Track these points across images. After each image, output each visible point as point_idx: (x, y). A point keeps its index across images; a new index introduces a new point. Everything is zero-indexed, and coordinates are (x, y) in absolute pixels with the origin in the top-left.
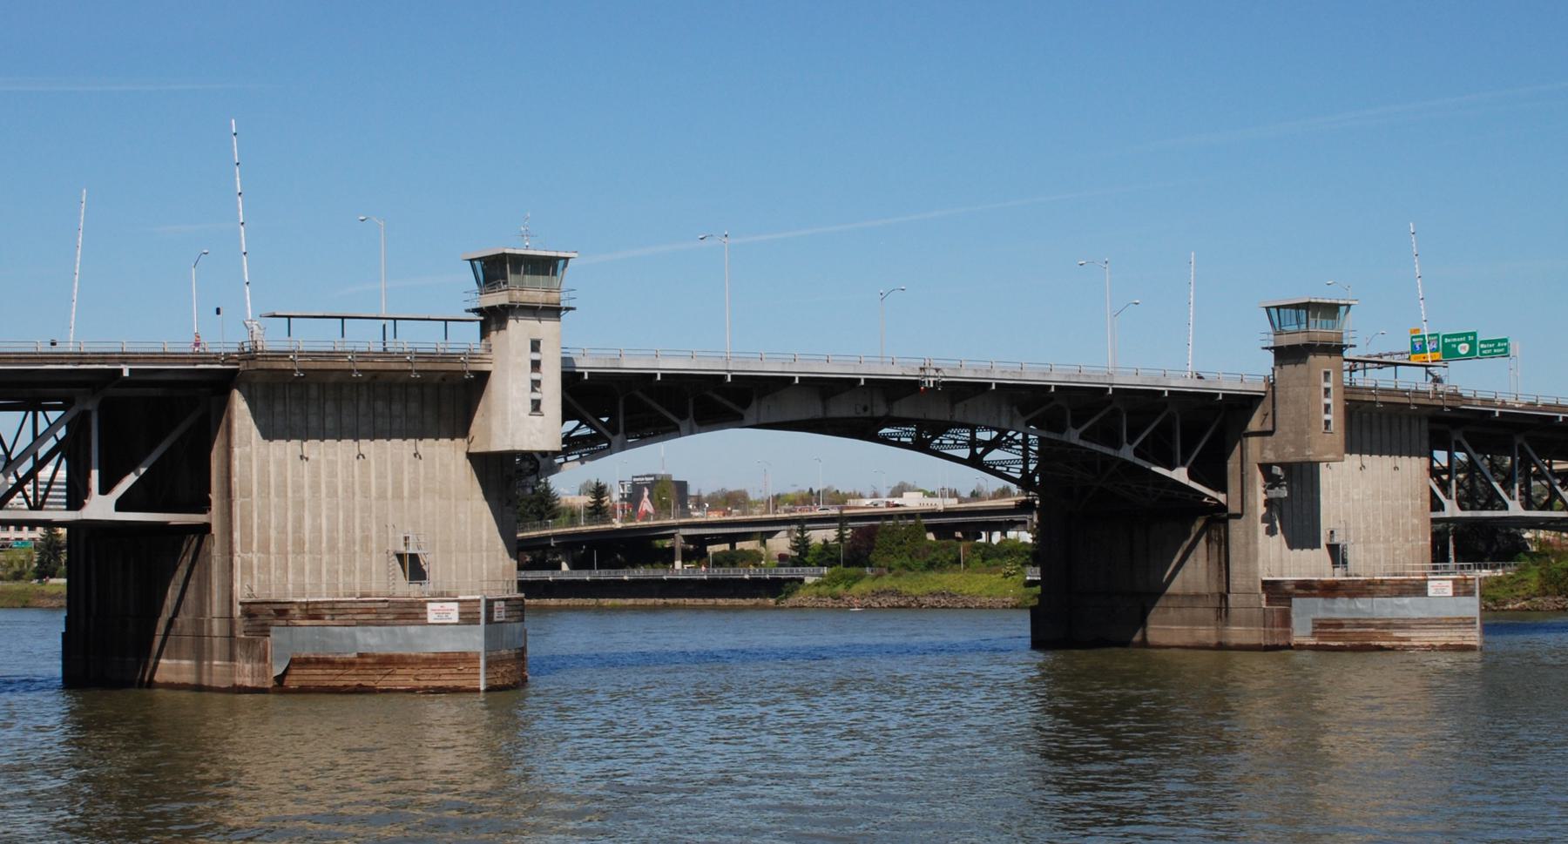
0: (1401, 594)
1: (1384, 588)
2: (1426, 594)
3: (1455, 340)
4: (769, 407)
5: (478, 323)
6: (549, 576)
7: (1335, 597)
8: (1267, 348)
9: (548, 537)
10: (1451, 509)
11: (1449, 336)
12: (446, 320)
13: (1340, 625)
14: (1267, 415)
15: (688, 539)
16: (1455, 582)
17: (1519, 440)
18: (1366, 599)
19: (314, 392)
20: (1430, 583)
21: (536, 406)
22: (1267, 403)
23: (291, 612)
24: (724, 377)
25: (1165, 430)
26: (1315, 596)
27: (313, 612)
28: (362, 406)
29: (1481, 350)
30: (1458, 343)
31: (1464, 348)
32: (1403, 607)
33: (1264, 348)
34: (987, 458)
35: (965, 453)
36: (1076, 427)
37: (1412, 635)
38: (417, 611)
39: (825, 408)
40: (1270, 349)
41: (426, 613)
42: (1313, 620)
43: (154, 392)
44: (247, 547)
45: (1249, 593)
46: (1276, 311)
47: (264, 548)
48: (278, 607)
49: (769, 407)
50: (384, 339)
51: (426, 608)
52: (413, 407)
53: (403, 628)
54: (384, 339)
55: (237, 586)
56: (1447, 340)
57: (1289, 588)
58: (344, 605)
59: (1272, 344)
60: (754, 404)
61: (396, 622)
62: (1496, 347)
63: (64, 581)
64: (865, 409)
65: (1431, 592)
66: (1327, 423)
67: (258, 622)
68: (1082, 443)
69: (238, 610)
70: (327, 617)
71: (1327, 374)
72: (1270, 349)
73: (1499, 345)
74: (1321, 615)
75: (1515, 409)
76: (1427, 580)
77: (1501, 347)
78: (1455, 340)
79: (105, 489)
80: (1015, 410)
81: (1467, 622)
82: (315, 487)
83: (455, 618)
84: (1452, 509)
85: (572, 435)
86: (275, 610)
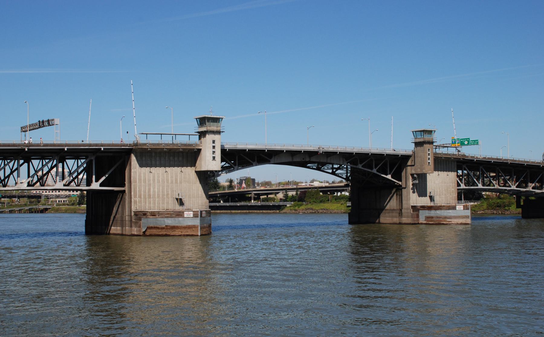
0: (449, 209)
1: (445, 207)
2: (456, 209)
3: (464, 140)
4: (277, 158)
5: (198, 136)
6: (217, 204)
7: (431, 210)
8: (412, 142)
9: (217, 194)
10: (463, 186)
11: (462, 139)
12: (189, 135)
13: (433, 218)
14: (412, 161)
15: (255, 194)
16: (464, 206)
17: (481, 167)
18: (439, 211)
19: (153, 154)
20: (457, 206)
21: (214, 158)
22: (413, 158)
23: (147, 214)
24: (265, 150)
25: (385, 165)
26: (425, 210)
27: (153, 214)
28: (167, 158)
29: (471, 143)
30: (464, 141)
31: (466, 142)
32: (450, 213)
33: (412, 142)
34: (337, 172)
35: (330, 171)
36: (361, 164)
37: (452, 220)
38: (182, 214)
39: (292, 159)
40: (414, 143)
41: (184, 214)
42: (425, 216)
43: (111, 154)
44: (135, 197)
45: (408, 209)
46: (415, 132)
47: (140, 197)
48: (144, 213)
49: (277, 158)
50: (173, 140)
51: (184, 213)
52: (181, 159)
53: (178, 218)
54: (173, 140)
55: (133, 207)
56: (461, 140)
57: (419, 208)
58: (161, 212)
59: (414, 141)
60: (273, 157)
61: (176, 217)
62: (475, 142)
63: (85, 206)
64: (303, 159)
65: (457, 209)
66: (429, 163)
67: (138, 217)
68: (362, 168)
69: (133, 214)
70: (157, 216)
71: (429, 149)
72: (414, 143)
73: (476, 141)
74: (427, 215)
75: (480, 159)
76: (456, 205)
77: (476, 142)
78: (464, 140)
79: (97, 181)
80: (344, 159)
81: (467, 217)
82: (154, 180)
83: (192, 216)
84: (463, 186)
85: (65, 162)
86: (143, 214)
